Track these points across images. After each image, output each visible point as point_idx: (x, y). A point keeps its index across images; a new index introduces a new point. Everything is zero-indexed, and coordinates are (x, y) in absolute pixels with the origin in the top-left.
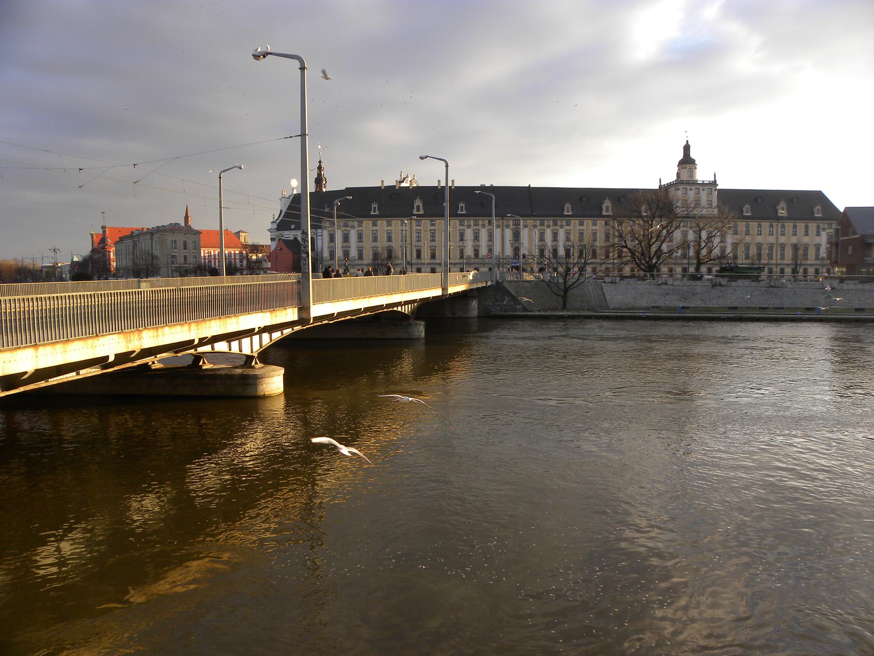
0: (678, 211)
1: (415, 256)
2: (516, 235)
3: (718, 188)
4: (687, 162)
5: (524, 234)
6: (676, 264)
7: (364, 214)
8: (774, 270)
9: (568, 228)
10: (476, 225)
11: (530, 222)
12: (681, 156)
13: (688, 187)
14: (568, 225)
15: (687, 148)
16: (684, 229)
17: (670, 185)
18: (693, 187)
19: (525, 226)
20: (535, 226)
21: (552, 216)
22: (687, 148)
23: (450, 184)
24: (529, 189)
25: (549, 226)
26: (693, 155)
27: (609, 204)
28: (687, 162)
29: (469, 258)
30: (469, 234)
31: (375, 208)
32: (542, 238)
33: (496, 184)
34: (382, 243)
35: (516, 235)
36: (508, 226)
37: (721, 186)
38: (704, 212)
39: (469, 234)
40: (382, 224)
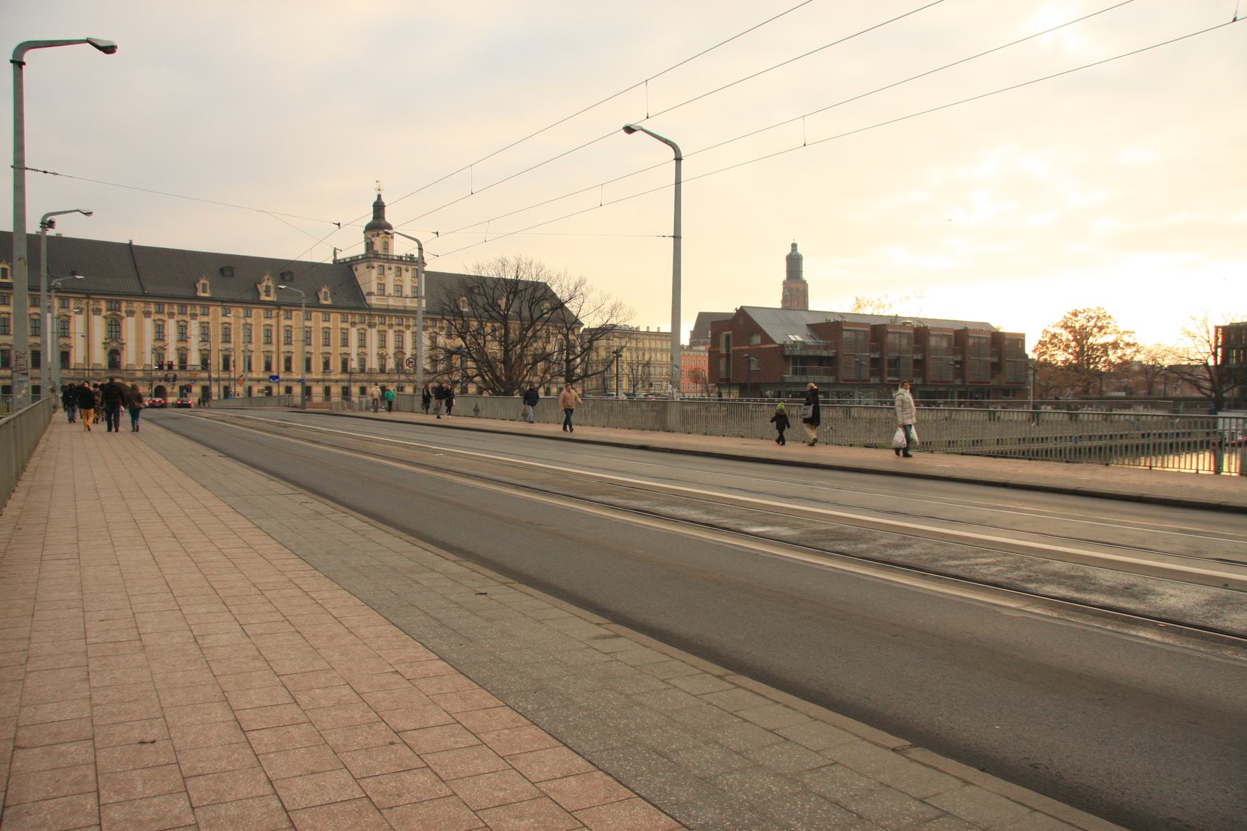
0: (374, 301)
1: (282, 368)
2: (114, 327)
3: (426, 269)
4: (378, 225)
5: (129, 325)
6: (370, 381)
7: (189, 299)
8: (169, 390)
9: (205, 319)
10: (159, 312)
11: (138, 306)
12: (369, 219)
13: (387, 266)
14: (205, 314)
15: (379, 207)
16: (381, 328)
17: (354, 261)
18: (393, 266)
19: (131, 313)
20: (147, 314)
21: (154, 296)
22: (379, 207)
23: (33, 227)
24: (130, 249)
25: (171, 315)
26: (389, 217)
27: (270, 284)
28: (378, 225)
29: (371, 372)
30: (171, 328)
31: (204, 285)
32: (160, 334)
33: (145, 238)
34: (278, 351)
35: (114, 327)
36: (97, 311)
37: (432, 266)
38: (392, 302)
39: (171, 328)
40: (216, 317)
